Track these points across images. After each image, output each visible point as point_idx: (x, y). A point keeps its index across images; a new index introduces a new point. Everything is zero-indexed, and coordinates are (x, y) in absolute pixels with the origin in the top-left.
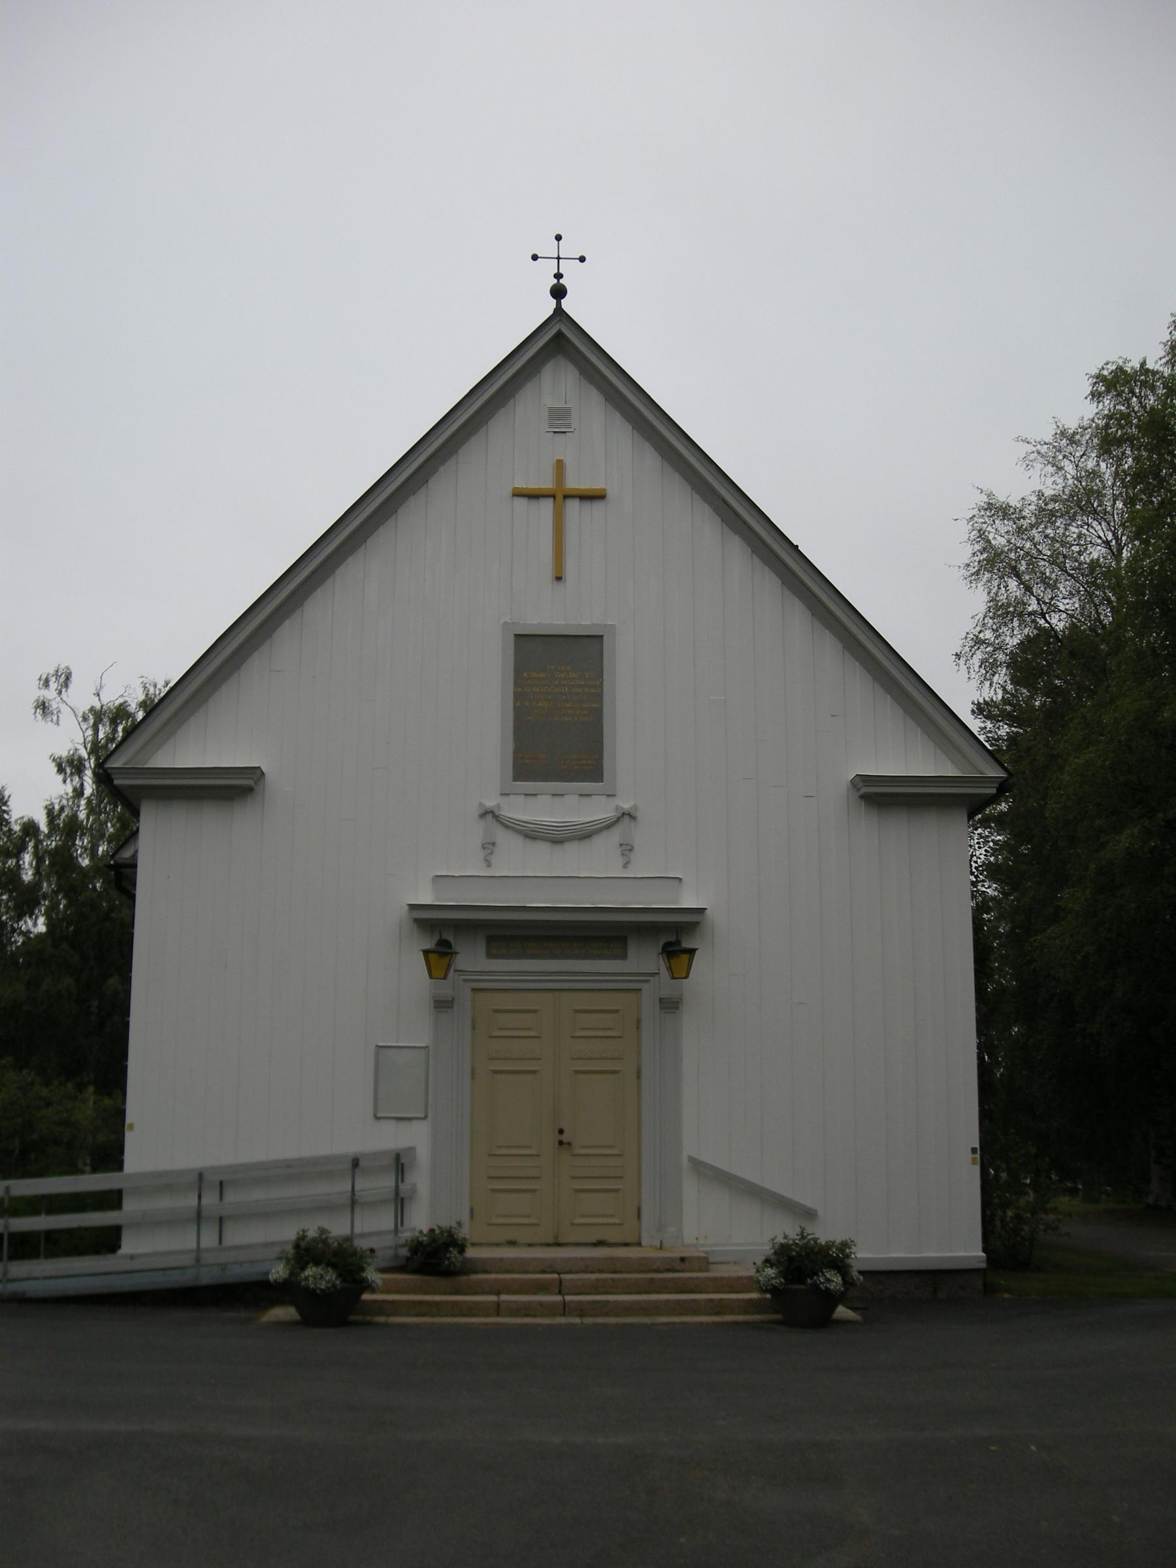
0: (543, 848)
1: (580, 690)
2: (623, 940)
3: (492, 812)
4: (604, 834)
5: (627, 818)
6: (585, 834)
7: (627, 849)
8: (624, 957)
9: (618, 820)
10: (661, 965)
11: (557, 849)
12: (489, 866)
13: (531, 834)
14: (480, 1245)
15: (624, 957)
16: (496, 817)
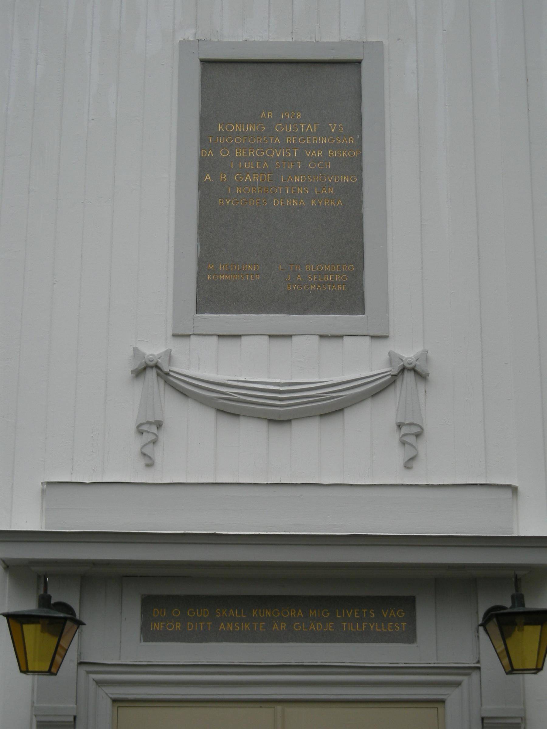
0: (251, 432)
1: (320, 154)
2: (408, 604)
3: (157, 366)
4: (368, 406)
5: (409, 377)
6: (330, 406)
7: (411, 433)
8: (410, 636)
9: (393, 380)
10: (486, 651)
11: (279, 433)
12: (150, 465)
13: (230, 405)
14: (400, 394)
15: (410, 636)
16: (165, 376)
